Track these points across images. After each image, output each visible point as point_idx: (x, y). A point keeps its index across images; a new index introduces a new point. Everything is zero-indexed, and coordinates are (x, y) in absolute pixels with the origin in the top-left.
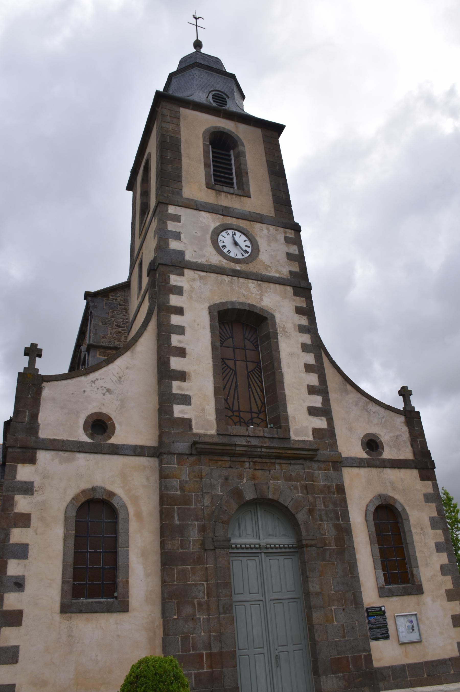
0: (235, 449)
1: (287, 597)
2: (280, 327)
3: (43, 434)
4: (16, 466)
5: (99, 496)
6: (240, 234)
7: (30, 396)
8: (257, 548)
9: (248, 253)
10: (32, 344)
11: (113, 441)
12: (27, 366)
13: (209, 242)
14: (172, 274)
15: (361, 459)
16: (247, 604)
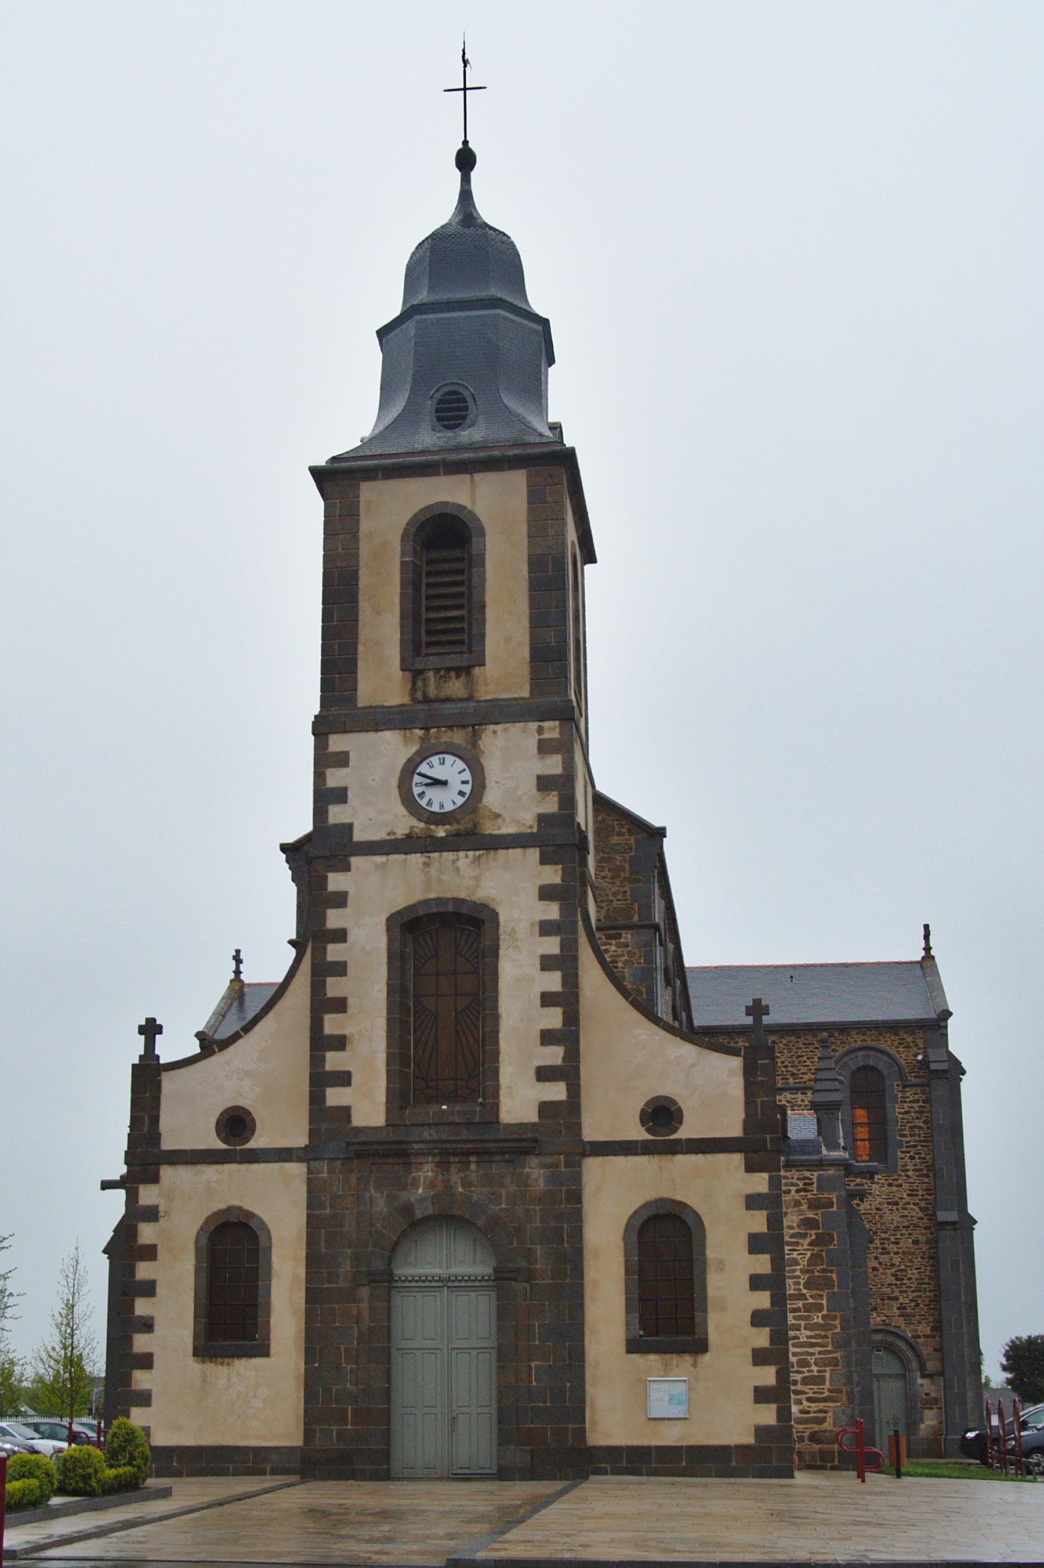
0: (311, 1163)
1: (479, 1345)
2: (505, 932)
3: (167, 1144)
4: (137, 1188)
5: (233, 1219)
6: (453, 758)
7: (148, 1095)
8: (437, 1281)
9: (464, 797)
10: (147, 1019)
11: (252, 1144)
12: (143, 1053)
13: (395, 793)
14: (331, 872)
15: (645, 1142)
16: (419, 1353)
